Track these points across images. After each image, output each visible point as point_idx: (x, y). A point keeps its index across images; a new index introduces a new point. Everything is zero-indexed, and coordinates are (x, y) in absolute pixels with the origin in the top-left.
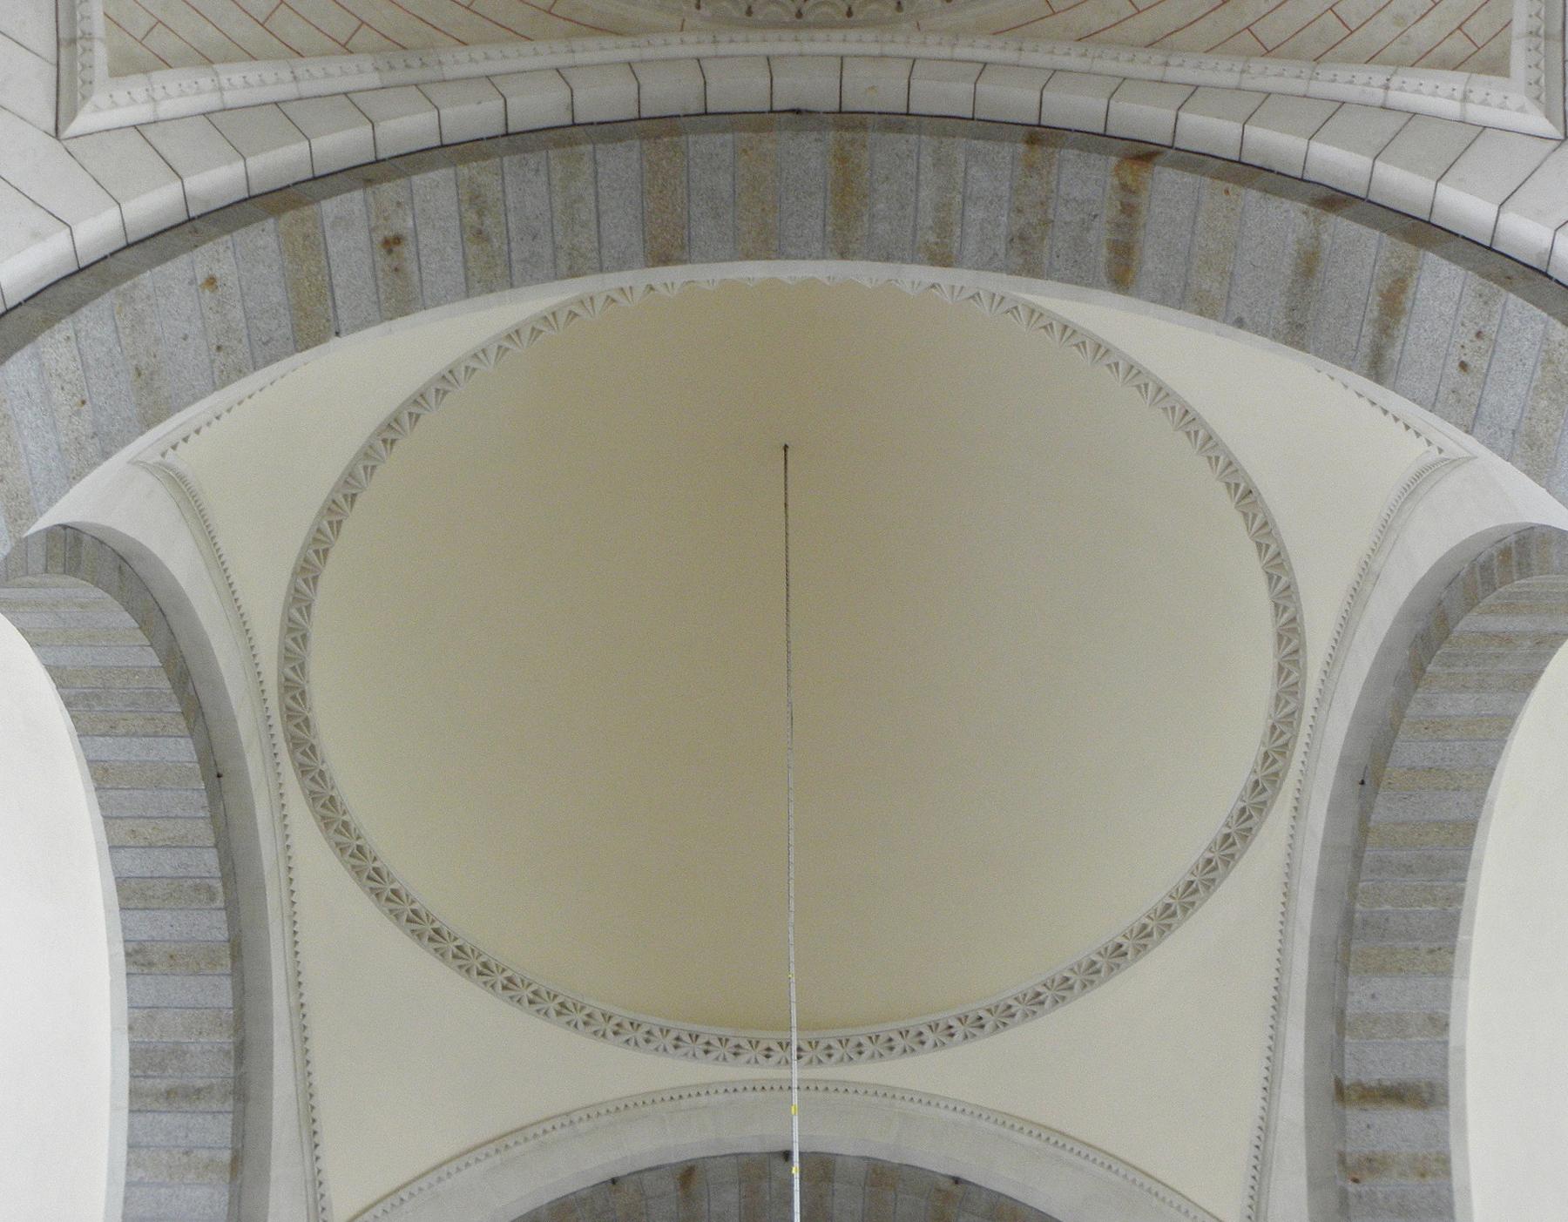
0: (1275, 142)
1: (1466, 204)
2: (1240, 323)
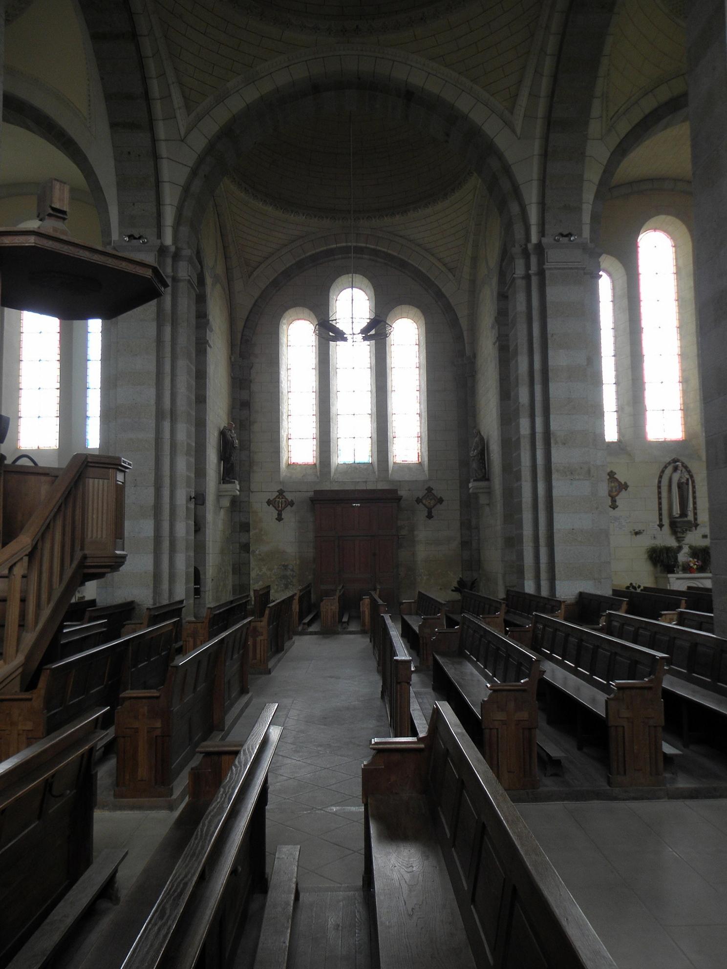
0: (152, 68)
1: (161, 131)
2: (102, 79)
